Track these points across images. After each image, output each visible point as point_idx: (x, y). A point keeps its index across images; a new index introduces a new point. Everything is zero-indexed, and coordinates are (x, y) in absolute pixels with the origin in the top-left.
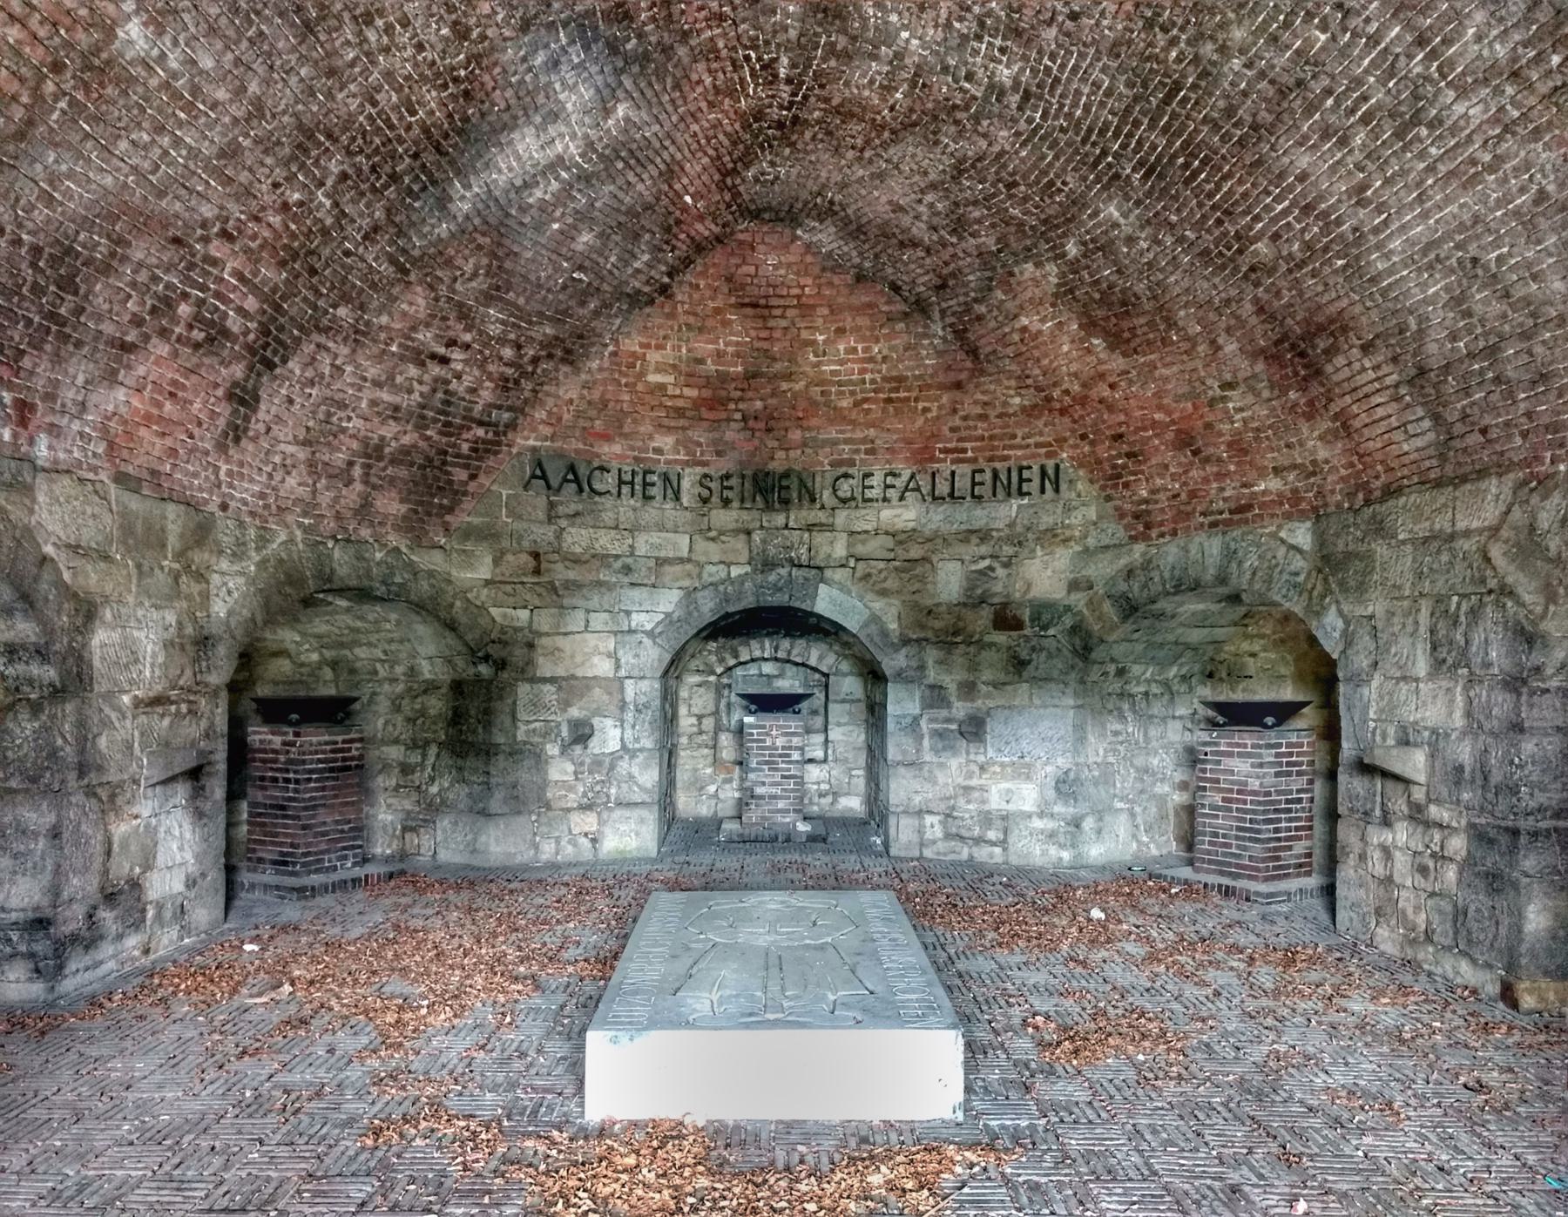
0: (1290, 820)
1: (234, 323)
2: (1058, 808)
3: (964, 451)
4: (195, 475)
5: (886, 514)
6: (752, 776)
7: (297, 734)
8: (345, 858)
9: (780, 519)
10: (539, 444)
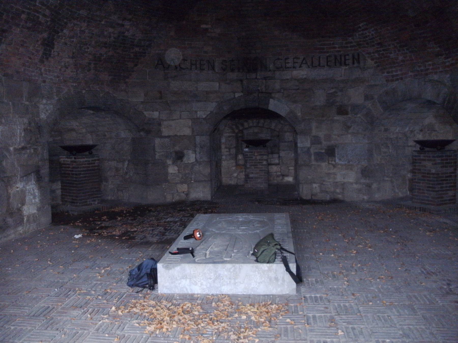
0: (447, 183)
1: (42, 19)
2: (363, 181)
3: (323, 49)
4: (33, 72)
5: (295, 73)
6: (248, 170)
7: (75, 158)
8: (95, 201)
9: (253, 76)
10: (160, 52)
